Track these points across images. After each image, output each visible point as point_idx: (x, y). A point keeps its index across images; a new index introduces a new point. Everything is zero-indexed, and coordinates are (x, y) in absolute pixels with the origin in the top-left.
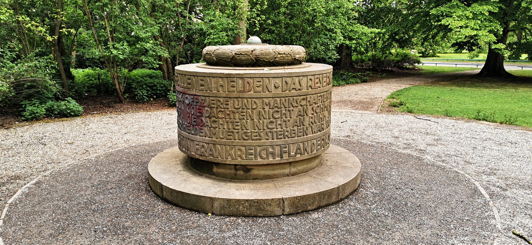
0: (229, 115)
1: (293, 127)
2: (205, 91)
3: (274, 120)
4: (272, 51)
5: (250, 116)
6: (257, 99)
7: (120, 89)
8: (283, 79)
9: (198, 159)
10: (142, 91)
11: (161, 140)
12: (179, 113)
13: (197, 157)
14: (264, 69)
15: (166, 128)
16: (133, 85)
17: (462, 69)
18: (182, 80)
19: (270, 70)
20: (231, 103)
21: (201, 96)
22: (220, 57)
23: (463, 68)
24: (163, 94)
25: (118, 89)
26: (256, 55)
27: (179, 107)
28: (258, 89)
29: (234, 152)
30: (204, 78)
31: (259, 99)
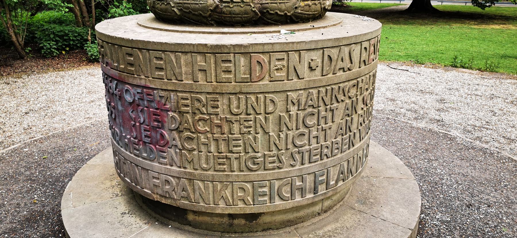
0: (219, 126)
1: (335, 138)
2: (166, 80)
3: (306, 131)
5: (262, 127)
6: (275, 94)
7: (18, 41)
8: (325, 52)
9: (157, 201)
10: (49, 42)
11: (82, 124)
12: (113, 116)
15: (87, 99)
16: (36, 34)
17: (387, 5)
18: (114, 55)
19: (293, 32)
20: (223, 104)
21: (157, 89)
22: (188, 8)
23: (388, 4)
24: (79, 45)
25: (16, 42)
26: (261, 4)
27: (113, 104)
28: (279, 74)
29: (231, 193)
30: (163, 55)
31: (279, 95)
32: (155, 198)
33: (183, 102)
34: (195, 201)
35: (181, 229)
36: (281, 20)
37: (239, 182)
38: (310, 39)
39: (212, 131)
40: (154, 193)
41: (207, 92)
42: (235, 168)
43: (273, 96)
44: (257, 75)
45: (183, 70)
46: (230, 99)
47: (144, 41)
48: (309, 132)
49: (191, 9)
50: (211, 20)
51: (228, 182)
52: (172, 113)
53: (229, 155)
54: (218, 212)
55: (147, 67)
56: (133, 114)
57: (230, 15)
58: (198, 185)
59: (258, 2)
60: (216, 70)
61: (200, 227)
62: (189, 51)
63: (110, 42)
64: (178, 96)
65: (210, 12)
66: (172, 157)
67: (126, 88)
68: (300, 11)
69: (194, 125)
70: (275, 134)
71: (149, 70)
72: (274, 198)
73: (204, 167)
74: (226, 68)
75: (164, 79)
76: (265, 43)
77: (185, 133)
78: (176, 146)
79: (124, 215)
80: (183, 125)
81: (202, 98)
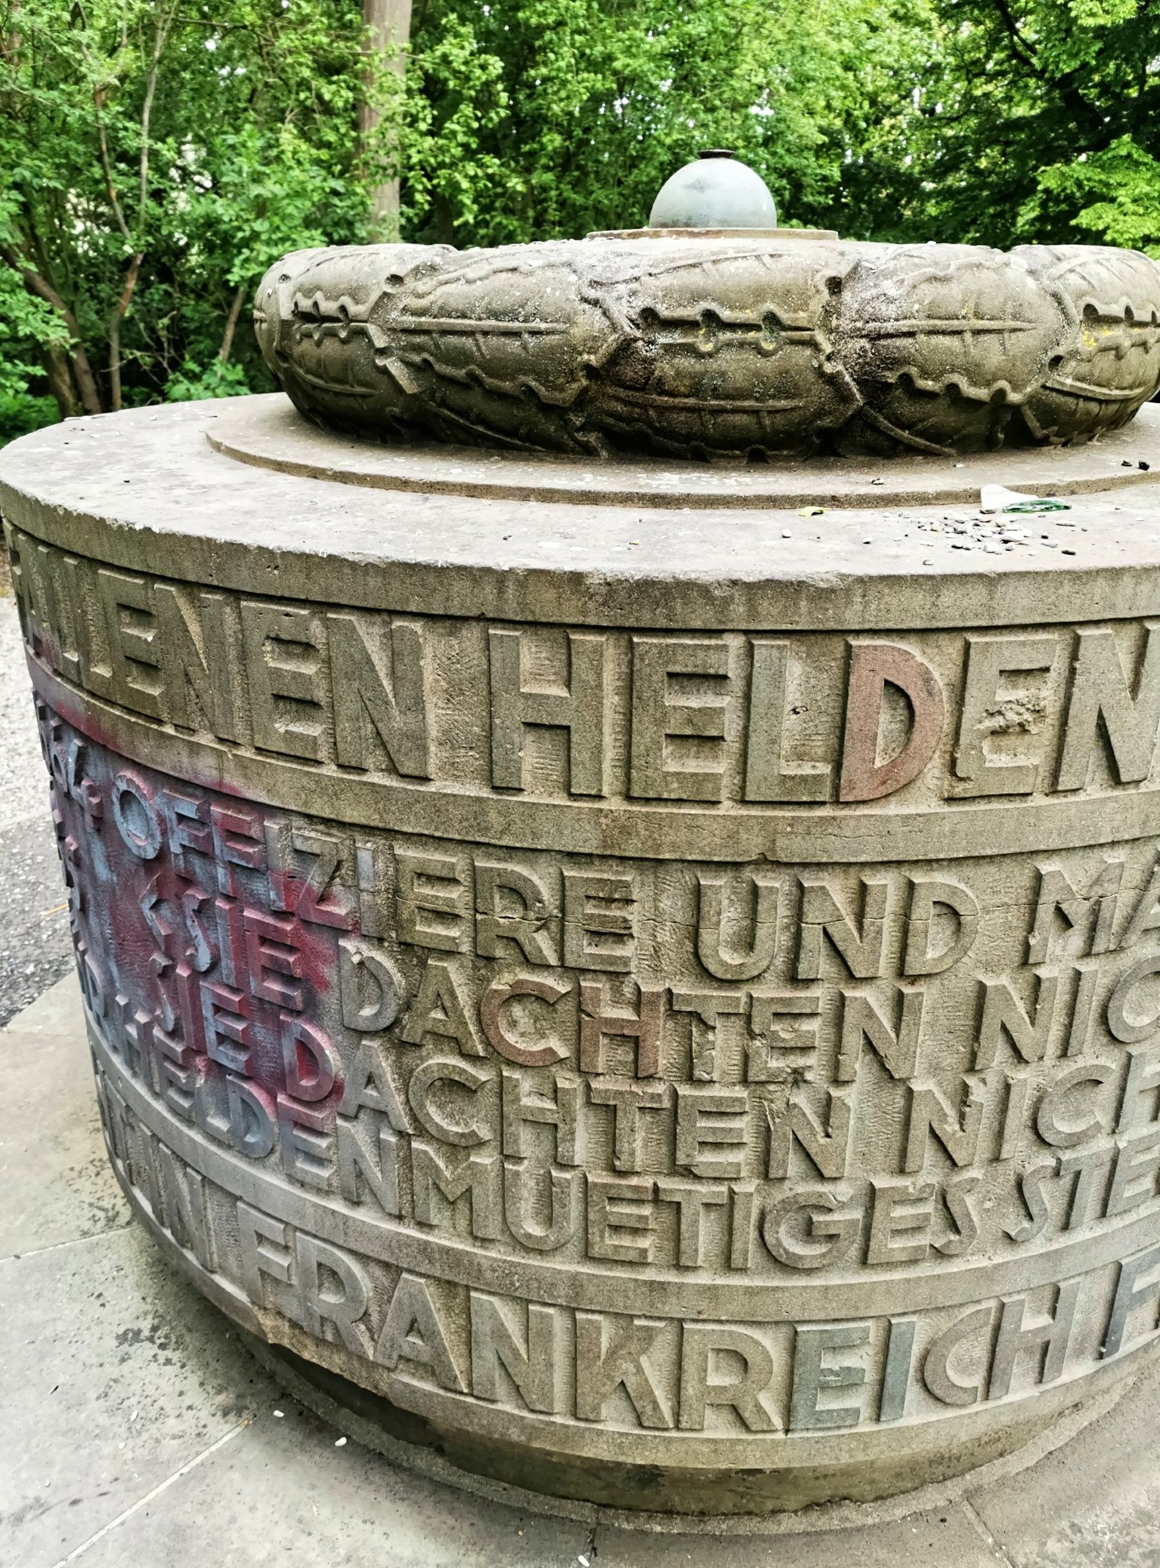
2: (330, 770)
3: (1112, 1061)
4: (1030, 282)
6: (969, 870)
13: (276, 1330)
14: (975, 497)
20: (657, 918)
22: (460, 358)
28: (1002, 760)
29: (668, 1368)
32: (267, 1330)
33: (425, 898)
34: (470, 1384)
35: (395, 1466)
36: (964, 432)
37: (720, 1322)
38: (799, 492)
39: (585, 1060)
40: (265, 1309)
41: (570, 849)
42: (701, 1250)
43: (954, 882)
44: (878, 764)
45: (431, 718)
46: (698, 892)
47: (209, 540)
48: (1127, 1068)
49: (479, 366)
50: (582, 428)
51: (660, 1319)
52: (364, 947)
53: (671, 1191)
54: (591, 1455)
55: (225, 690)
56: (160, 917)
57: (691, 401)
58: (494, 1315)
59: (859, 324)
60: (628, 730)
61: (491, 1470)
62: (474, 612)
63: (41, 535)
64: (396, 860)
65: (585, 382)
66: (355, 1162)
67: (123, 786)
68: (1069, 381)
69: (486, 1019)
70: (940, 1084)
71: (238, 703)
72: (898, 1401)
73: (529, 1236)
74: (690, 721)
75: (319, 763)
76: (948, 571)
77: (428, 1057)
78: (381, 1115)
79: (131, 1350)
80: (424, 1015)
81: (535, 878)
